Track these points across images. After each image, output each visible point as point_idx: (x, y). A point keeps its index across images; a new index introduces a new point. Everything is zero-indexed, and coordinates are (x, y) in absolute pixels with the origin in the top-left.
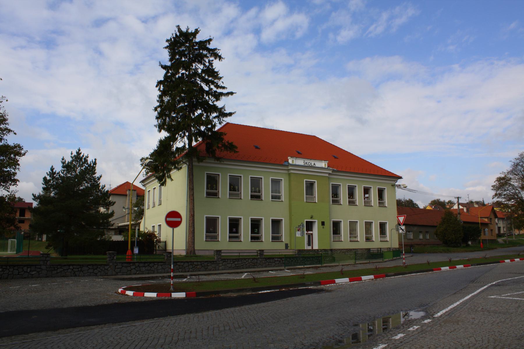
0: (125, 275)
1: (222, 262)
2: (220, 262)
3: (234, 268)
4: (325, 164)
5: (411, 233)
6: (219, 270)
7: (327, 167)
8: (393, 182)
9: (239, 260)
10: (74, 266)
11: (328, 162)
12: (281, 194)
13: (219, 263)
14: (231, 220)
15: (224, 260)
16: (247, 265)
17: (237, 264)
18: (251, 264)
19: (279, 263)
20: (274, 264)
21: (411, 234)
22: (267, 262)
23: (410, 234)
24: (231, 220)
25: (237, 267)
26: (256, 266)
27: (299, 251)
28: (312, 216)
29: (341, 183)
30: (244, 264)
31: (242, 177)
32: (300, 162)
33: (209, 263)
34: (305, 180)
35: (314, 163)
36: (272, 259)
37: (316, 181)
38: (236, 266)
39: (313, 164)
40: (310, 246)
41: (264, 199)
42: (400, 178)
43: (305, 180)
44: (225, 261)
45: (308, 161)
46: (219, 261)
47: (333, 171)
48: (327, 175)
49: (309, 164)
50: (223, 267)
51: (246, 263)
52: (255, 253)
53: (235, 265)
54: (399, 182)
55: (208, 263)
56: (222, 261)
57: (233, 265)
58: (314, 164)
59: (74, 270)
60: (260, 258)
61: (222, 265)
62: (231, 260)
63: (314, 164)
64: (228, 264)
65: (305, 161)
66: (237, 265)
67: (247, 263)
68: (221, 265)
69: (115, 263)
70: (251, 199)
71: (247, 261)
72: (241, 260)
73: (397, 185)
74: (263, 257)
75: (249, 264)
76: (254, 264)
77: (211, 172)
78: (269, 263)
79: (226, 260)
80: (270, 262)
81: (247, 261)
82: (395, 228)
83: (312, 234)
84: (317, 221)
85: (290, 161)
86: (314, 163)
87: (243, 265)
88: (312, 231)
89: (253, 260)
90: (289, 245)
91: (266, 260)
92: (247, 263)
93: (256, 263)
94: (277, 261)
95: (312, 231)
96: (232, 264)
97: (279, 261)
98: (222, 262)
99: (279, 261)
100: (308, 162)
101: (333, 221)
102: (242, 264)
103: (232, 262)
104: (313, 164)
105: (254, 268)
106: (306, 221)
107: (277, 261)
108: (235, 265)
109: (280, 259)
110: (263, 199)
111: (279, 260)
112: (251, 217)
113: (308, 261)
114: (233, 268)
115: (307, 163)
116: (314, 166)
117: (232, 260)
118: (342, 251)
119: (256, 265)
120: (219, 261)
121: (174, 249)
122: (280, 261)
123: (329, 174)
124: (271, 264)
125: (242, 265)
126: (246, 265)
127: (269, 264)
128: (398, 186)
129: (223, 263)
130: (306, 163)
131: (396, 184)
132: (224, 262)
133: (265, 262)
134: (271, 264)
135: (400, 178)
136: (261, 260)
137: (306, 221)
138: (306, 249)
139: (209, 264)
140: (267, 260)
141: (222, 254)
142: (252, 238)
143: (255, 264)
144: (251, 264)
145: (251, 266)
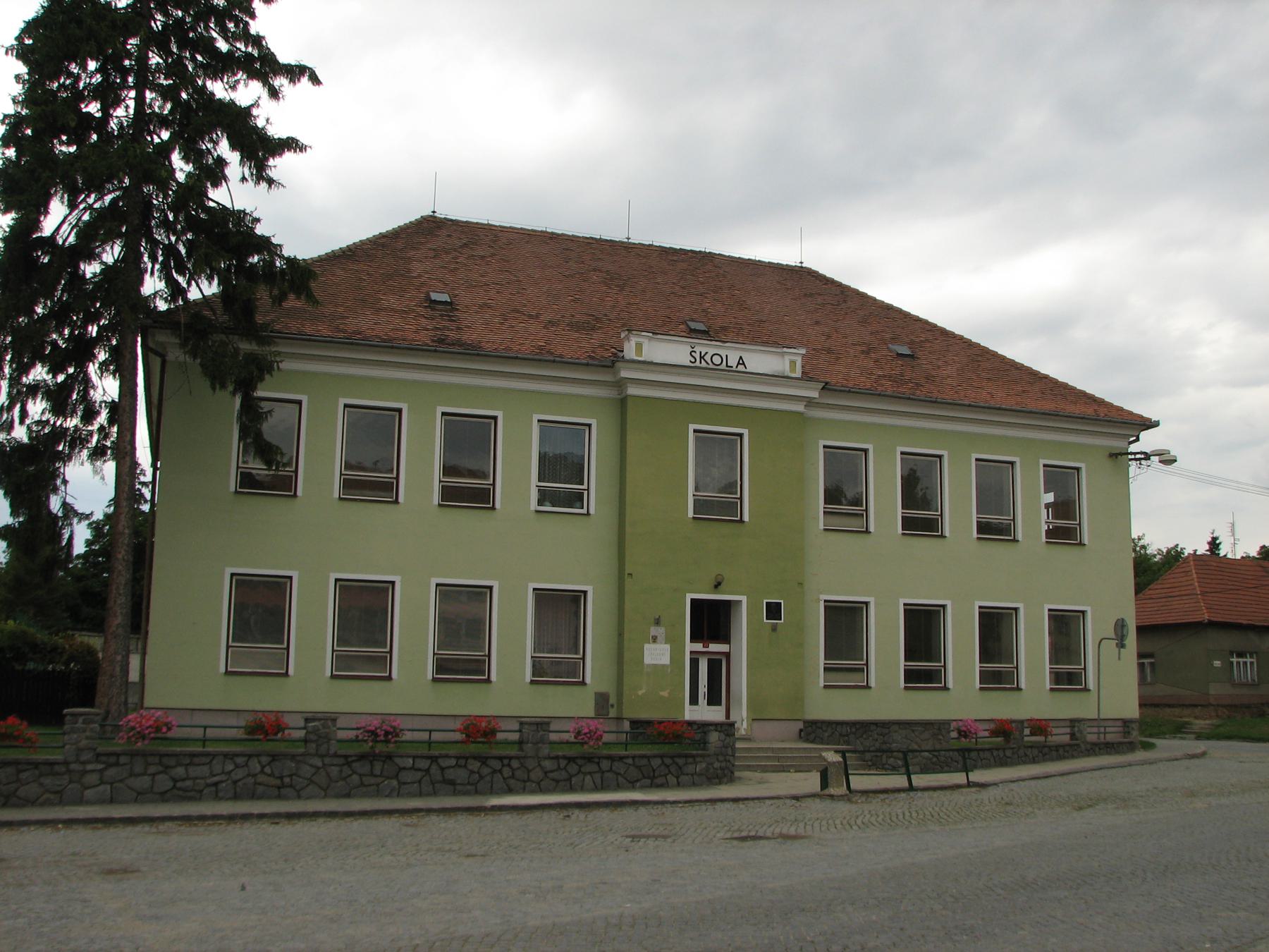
0: (228, 799)
1: (100, 766)
2: (89, 767)
3: (164, 797)
4: (793, 363)
5: (1249, 660)
6: (81, 801)
7: (798, 374)
8: (1117, 444)
9: (196, 760)
10: (665, 759)
11: (803, 351)
12: (585, 487)
13: (85, 772)
14: (243, 584)
15: (113, 759)
16: (240, 783)
17: (184, 780)
18: (261, 778)
19: (420, 782)
20: (395, 783)
21: (1252, 663)
22: (354, 772)
23: (1245, 663)
24: (243, 584)
25: (185, 790)
26: (288, 789)
27: (807, 725)
28: (719, 579)
29: (303, 393)
30: (223, 777)
31: (1084, 474)
32: (673, 351)
33: (25, 771)
34: (692, 427)
35: (741, 358)
36: (384, 762)
37: (745, 432)
38: (174, 787)
39: (733, 362)
40: (719, 704)
41: (1089, 541)
42: (1149, 424)
43: (692, 427)
44: (117, 764)
45: (707, 348)
46: (84, 763)
47: (826, 388)
48: (800, 408)
49: (717, 360)
50: (101, 788)
51: (234, 776)
52: (421, 733)
53: (175, 781)
54: (1148, 441)
55: (19, 771)
56: (98, 761)
57: (164, 782)
58: (741, 362)
59: (607, 775)
60: (316, 755)
61: (102, 783)
62: (150, 759)
63: (741, 362)
64: (131, 775)
65: (698, 349)
66: (179, 785)
67: (240, 774)
68: (92, 778)
69: (550, 758)
70: (903, 534)
71: (237, 766)
72: (207, 760)
73: (1135, 454)
74: (332, 752)
75: (251, 780)
76: (281, 778)
77: (279, 391)
78: (367, 780)
79: (123, 760)
80: (372, 774)
81: (237, 766)
82: (1114, 637)
83: (728, 655)
84: (744, 599)
85: (630, 351)
86: (741, 358)
87: (216, 784)
88: (726, 639)
89: (273, 760)
90: (612, 700)
91: (349, 764)
92: (240, 774)
93: (290, 776)
94: (413, 768)
95: (726, 639)
96: (154, 775)
97: (419, 770)
98: (100, 766)
99: (419, 770)
100: (711, 352)
101: (825, 601)
102: (209, 781)
103: (152, 769)
104: (733, 362)
105: (279, 797)
106: (693, 601)
107: (413, 768)
108: (175, 781)
109: (428, 762)
110: (947, 533)
111: (424, 764)
112: (233, 566)
113: (585, 774)
114: (163, 794)
115: (708, 358)
116: (741, 368)
117: (157, 760)
118: (839, 728)
119: (291, 786)
120: (84, 763)
121: (1096, 717)
122: (427, 771)
123: (810, 402)
124: (378, 785)
125: (208, 785)
126: (235, 782)
127: (362, 784)
128: (1139, 459)
129: (105, 769)
130: (701, 357)
131: (1133, 448)
132: (109, 765)
133: (341, 771)
134: (378, 785)
135: (1149, 424)
136: (317, 762)
137: (693, 601)
138: (687, 717)
139: (23, 776)
140: (354, 765)
141: (551, 734)
142: (911, 676)
143: (287, 780)
144: (261, 778)
145: (260, 789)
